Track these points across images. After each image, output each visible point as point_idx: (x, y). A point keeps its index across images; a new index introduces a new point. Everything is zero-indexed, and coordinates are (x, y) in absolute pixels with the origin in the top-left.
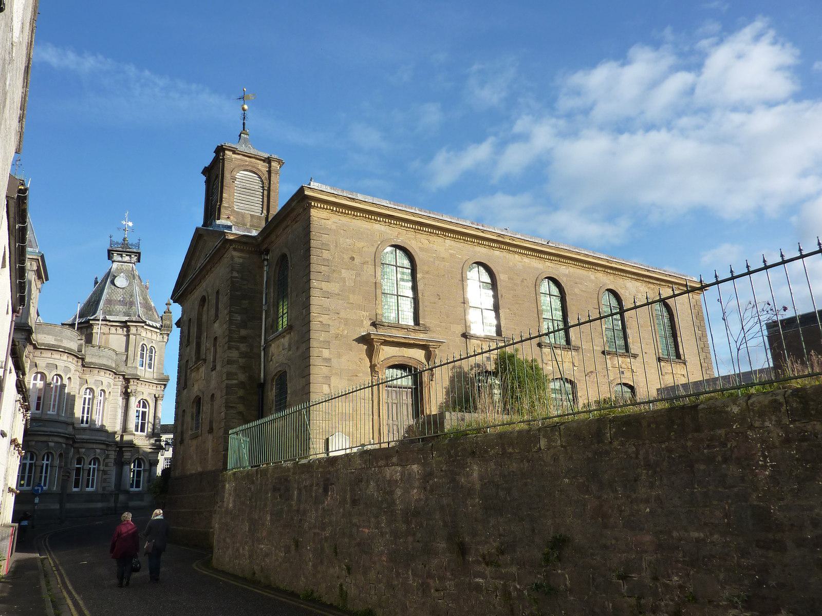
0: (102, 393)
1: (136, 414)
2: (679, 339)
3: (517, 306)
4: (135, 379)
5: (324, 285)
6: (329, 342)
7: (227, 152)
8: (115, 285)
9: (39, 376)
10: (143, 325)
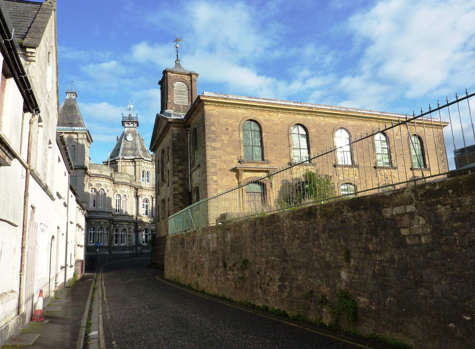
0: (125, 196)
1: (142, 206)
2: (426, 157)
3: (322, 145)
4: (141, 188)
5: (213, 144)
6: (216, 172)
7: (168, 73)
8: (127, 140)
9: (93, 190)
10: (142, 160)
